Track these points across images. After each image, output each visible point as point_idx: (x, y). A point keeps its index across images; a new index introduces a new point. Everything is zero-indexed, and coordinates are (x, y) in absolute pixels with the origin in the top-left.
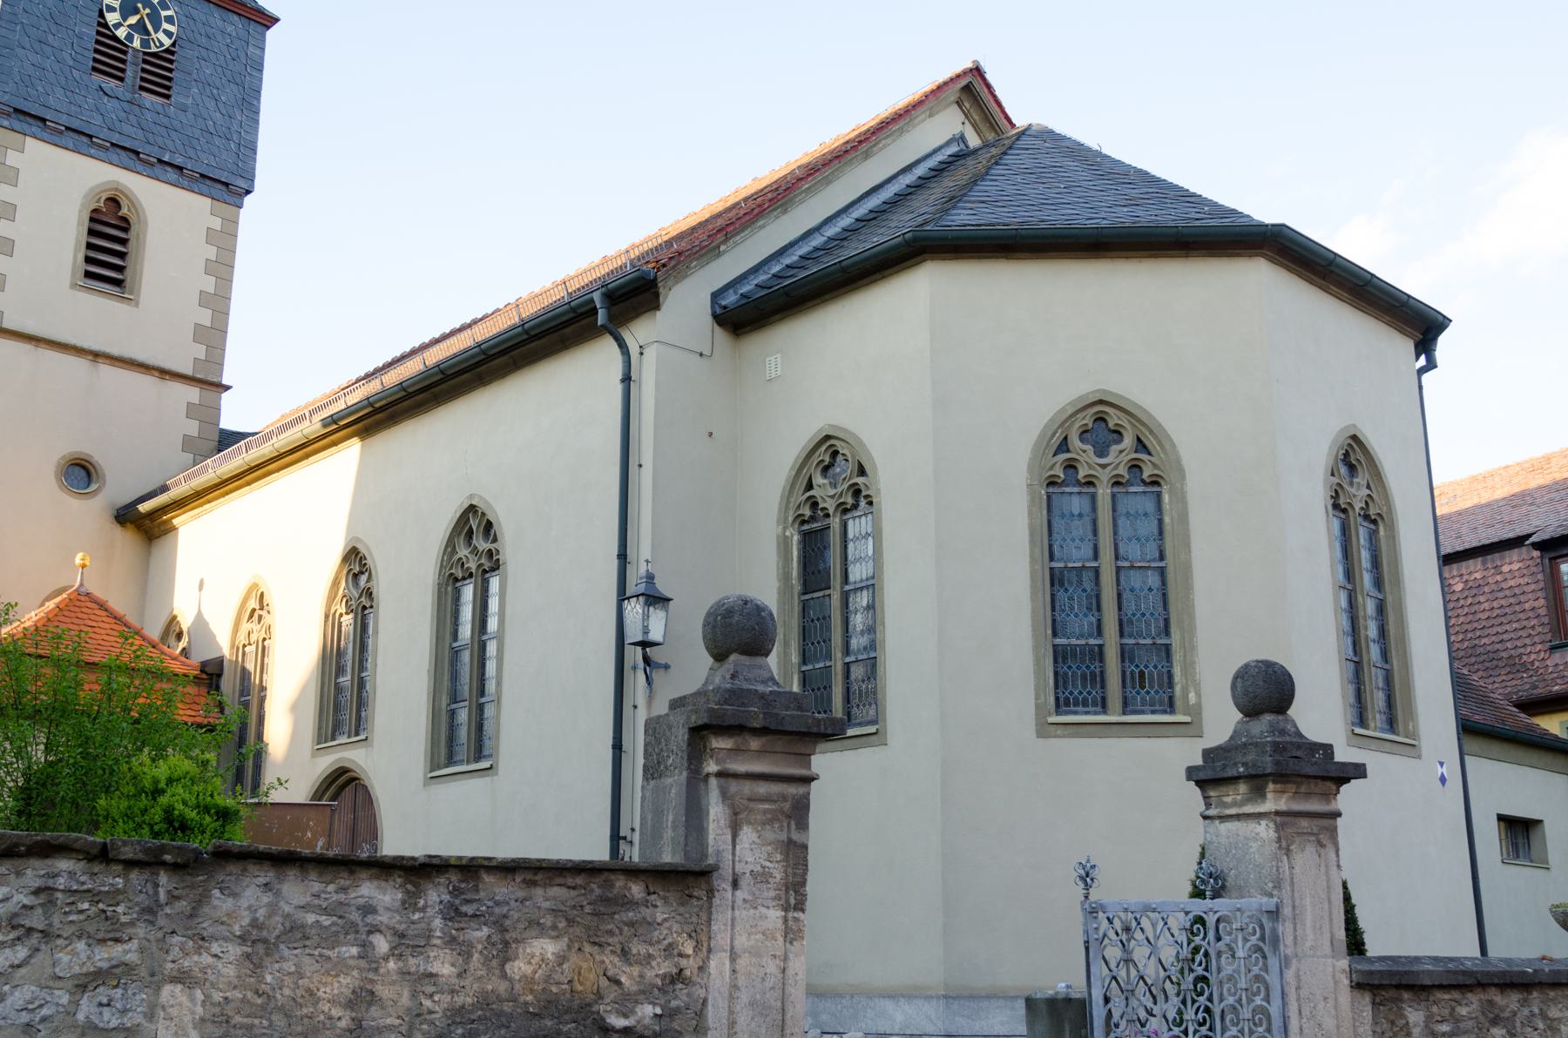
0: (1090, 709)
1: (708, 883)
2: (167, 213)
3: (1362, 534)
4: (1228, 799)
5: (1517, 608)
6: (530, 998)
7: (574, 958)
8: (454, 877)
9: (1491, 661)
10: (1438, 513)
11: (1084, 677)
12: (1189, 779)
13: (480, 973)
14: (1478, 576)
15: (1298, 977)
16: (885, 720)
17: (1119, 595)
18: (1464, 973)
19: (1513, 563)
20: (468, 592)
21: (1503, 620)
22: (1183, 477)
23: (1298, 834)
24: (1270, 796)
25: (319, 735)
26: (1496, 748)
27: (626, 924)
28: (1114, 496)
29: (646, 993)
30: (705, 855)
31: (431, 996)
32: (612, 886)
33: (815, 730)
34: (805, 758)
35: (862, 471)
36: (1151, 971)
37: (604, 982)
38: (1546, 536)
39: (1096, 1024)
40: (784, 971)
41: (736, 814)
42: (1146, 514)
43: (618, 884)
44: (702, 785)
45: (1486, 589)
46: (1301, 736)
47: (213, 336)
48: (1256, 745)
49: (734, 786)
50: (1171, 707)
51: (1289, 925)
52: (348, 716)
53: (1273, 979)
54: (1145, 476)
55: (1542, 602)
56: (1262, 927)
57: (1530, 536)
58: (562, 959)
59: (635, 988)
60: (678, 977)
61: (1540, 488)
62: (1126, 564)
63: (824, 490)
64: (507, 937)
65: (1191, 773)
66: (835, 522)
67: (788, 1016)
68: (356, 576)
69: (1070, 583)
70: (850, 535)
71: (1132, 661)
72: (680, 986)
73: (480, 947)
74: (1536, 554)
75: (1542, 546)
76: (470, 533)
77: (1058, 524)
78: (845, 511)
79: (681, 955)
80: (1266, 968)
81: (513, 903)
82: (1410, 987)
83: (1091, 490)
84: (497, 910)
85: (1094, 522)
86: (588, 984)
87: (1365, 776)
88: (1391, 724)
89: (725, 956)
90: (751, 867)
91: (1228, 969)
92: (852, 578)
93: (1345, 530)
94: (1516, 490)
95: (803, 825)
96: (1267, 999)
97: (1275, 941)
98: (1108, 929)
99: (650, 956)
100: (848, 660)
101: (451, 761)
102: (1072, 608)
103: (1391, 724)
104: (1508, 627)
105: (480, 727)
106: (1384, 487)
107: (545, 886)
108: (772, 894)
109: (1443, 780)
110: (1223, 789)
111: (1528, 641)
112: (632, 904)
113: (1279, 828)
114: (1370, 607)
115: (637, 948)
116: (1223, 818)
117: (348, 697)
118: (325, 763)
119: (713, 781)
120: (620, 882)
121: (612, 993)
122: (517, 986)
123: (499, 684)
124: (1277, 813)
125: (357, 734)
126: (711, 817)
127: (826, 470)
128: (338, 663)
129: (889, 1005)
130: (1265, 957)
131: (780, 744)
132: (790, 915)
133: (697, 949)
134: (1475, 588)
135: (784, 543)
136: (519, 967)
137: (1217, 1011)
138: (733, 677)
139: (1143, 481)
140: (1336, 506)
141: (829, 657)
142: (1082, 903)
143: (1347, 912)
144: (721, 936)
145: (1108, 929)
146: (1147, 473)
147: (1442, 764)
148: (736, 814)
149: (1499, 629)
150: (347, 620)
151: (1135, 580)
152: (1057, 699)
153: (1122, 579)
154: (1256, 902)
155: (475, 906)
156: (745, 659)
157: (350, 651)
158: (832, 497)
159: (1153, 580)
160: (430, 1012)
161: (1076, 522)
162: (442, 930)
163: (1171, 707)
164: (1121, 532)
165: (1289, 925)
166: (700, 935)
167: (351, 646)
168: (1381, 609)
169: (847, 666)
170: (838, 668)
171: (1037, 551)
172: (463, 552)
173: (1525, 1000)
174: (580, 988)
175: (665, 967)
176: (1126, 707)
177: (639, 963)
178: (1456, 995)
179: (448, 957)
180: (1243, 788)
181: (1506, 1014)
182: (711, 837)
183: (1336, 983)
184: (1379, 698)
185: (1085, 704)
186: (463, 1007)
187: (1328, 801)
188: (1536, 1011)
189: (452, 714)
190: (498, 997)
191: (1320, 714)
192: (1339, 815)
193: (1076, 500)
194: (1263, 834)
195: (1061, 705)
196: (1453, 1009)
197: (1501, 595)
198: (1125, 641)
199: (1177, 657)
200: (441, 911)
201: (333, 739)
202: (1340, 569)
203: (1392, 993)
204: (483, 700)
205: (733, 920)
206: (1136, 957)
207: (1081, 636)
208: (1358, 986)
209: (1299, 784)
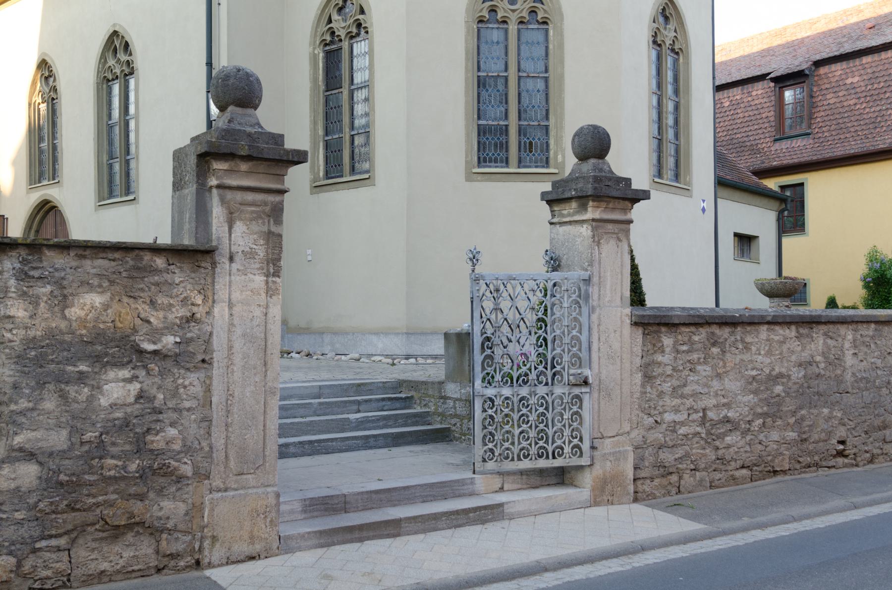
0: (499, 164)
1: (212, 258)
3: (669, 61)
4: (565, 212)
5: (758, 117)
6: (84, 332)
7: (116, 306)
8: (23, 252)
9: (741, 147)
10: (716, 61)
11: (496, 145)
12: (542, 199)
13: (46, 316)
14: (738, 97)
15: (599, 319)
16: (374, 170)
17: (519, 94)
18: (699, 316)
19: (759, 90)
20: (116, 89)
21: (750, 124)
22: (562, 19)
23: (605, 233)
24: (590, 209)
25: (30, 180)
26: (738, 195)
27: (153, 284)
28: (519, 30)
29: (169, 328)
30: (210, 240)
31: (11, 330)
32: (142, 259)
33: (285, 158)
34: (281, 177)
35: (362, 12)
36: (512, 316)
37: (138, 322)
38: (778, 74)
39: (475, 347)
40: (266, 314)
41: (231, 213)
42: (538, 43)
43: (146, 258)
44: (207, 194)
45: (742, 105)
46: (612, 172)
48: (584, 178)
49: (229, 195)
50: (547, 164)
51: (596, 288)
52: (48, 167)
53: (584, 319)
54: (539, 18)
55: (772, 113)
56: (580, 290)
57: (769, 74)
58: (106, 307)
59: (161, 325)
60: (192, 318)
61: (779, 46)
62: (525, 74)
63: (340, 25)
64: (65, 292)
65: (544, 195)
66: (345, 45)
67: (269, 343)
68: (46, 78)
69: (490, 86)
70: (355, 53)
71: (525, 135)
72: (193, 324)
73: (45, 298)
74: (772, 84)
75: (776, 80)
76: (115, 51)
77: (483, 47)
78: (352, 37)
79: (193, 304)
80: (580, 314)
81: (68, 270)
82: (666, 325)
83: (505, 26)
84: (57, 274)
85: (506, 47)
86: (127, 323)
87: (649, 198)
88: (677, 177)
89: (225, 306)
90: (243, 248)
91: (558, 314)
92: (355, 81)
93: (659, 57)
94: (765, 47)
95: (278, 221)
96: (580, 332)
97: (587, 297)
98: (485, 289)
99: (171, 305)
100: (353, 133)
101: (111, 195)
102: (490, 102)
103: (677, 177)
104: (752, 128)
105: (128, 175)
106: (685, 32)
107: (92, 259)
108: (257, 266)
109: (704, 210)
110: (563, 206)
111: (762, 136)
112: (157, 271)
113: (594, 229)
114: (670, 106)
115: (161, 300)
116: (561, 224)
117: (47, 157)
118: (36, 197)
119: (215, 191)
120: (147, 257)
121: (145, 328)
122: (74, 324)
123: (137, 147)
124: (593, 220)
125: (54, 179)
126: (214, 215)
127: (340, 10)
128: (39, 134)
129: (374, 338)
130: (580, 307)
131: (262, 167)
132: (270, 279)
133: (205, 300)
134: (735, 105)
135: (314, 58)
136: (74, 312)
137: (549, 338)
138: (230, 121)
139: (537, 21)
140: (655, 42)
141: (341, 131)
142: (471, 275)
143: (633, 283)
144: (222, 292)
145: (485, 289)
146: (540, 15)
147: (704, 201)
148: (231, 213)
149: (747, 129)
150: (43, 107)
151: (529, 84)
152: (479, 158)
153: (522, 84)
154: (577, 274)
155: (40, 271)
156: (239, 110)
157: (46, 127)
158: (343, 28)
159: (541, 85)
160: (11, 341)
161: (495, 47)
162: (16, 287)
163: (547, 164)
164: (522, 54)
165: (596, 288)
166: (208, 293)
167: (46, 124)
168: (677, 108)
169: (352, 137)
170: (347, 138)
171: (470, 64)
172: (111, 62)
173: (733, 332)
174: (120, 325)
175: (182, 312)
176: (520, 163)
177: (163, 309)
178: (693, 329)
179: (22, 305)
180: (574, 204)
181: (721, 340)
182: (214, 228)
183: (622, 322)
184: (670, 164)
185: (496, 161)
186: (34, 338)
187: (626, 214)
188: (739, 338)
189: (111, 166)
190: (60, 331)
191: (630, 160)
192: (632, 222)
193: (495, 32)
194: (584, 234)
195: (482, 161)
196: (690, 337)
197: (750, 109)
198: (521, 123)
199: (552, 133)
200: (14, 275)
201: (40, 182)
202: (654, 82)
203: (655, 328)
204: (128, 157)
205: (230, 282)
206: (502, 306)
207: (495, 119)
208: (636, 324)
209: (608, 203)
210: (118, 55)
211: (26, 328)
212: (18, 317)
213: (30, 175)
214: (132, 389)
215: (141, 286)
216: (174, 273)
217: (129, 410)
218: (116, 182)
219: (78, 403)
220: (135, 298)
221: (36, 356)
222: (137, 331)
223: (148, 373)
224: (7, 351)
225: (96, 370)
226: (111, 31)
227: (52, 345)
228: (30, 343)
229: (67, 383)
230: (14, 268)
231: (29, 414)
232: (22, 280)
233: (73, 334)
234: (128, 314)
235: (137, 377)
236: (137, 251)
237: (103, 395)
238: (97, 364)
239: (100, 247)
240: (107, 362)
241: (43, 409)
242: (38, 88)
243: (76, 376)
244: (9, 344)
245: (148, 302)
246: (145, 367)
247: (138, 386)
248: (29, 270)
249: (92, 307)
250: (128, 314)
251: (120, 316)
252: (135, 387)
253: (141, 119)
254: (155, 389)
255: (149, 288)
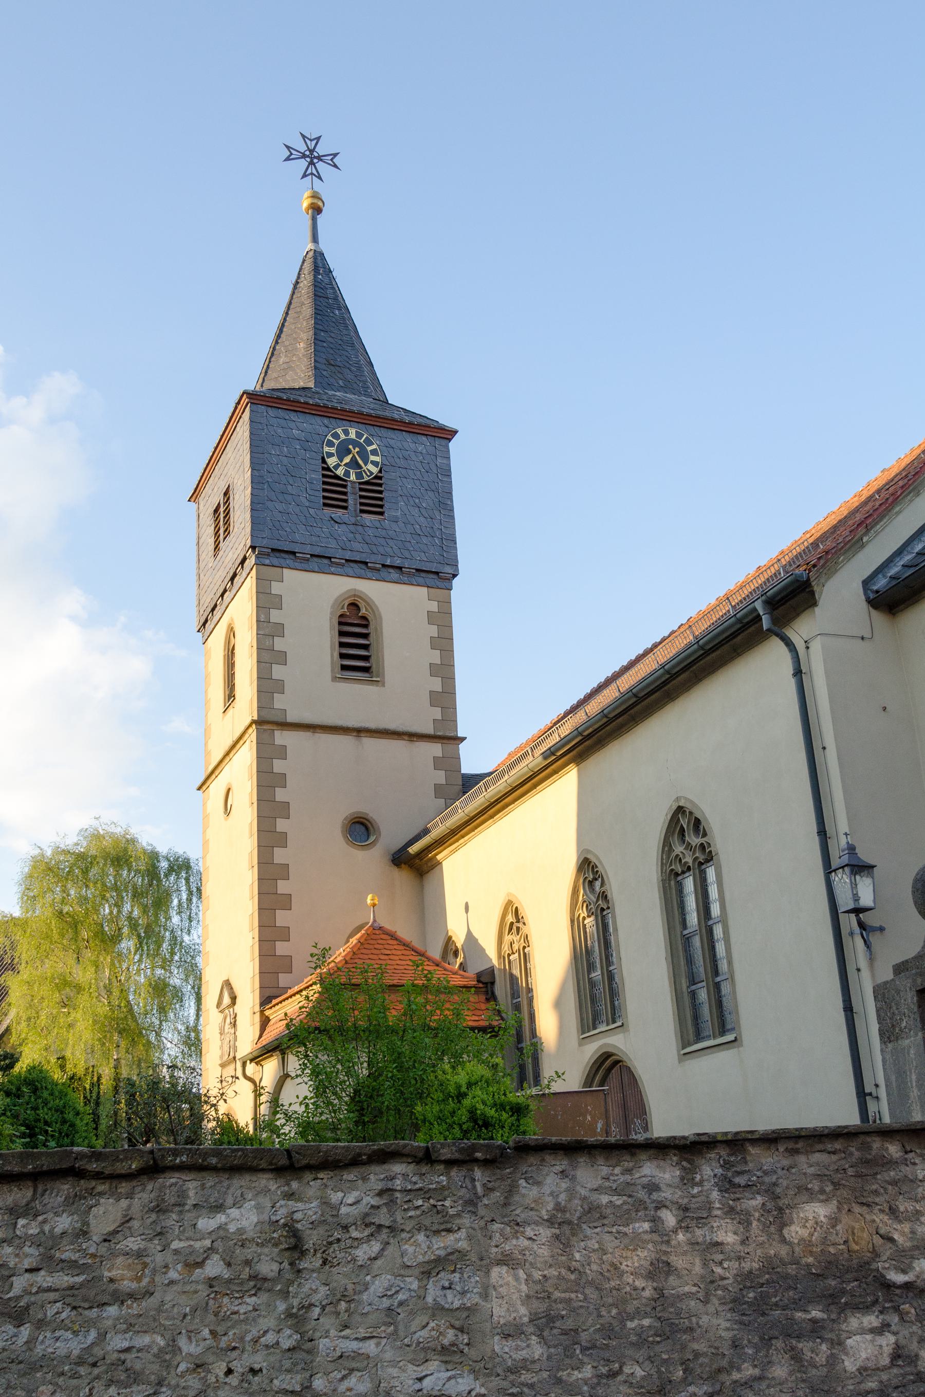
2: (395, 604)
6: (810, 1260)
7: (846, 1219)
8: (723, 1152)
20: (689, 884)
27: (890, 1183)
31: (721, 1263)
32: (870, 1148)
37: (878, 1240)
47: (445, 699)
52: (604, 1006)
58: (834, 1221)
59: (909, 1244)
64: (781, 1203)
84: (767, 1179)
86: (863, 1243)
101: (699, 1038)
105: (720, 1004)
107: (807, 1153)
112: (891, 1163)
115: (903, 1205)
117: (602, 990)
118: (592, 1050)
122: (797, 1249)
123: (730, 963)
125: (614, 1022)
128: (588, 961)
136: (796, 1232)
150: (590, 921)
155: (746, 1177)
160: (723, 1279)
172: (679, 849)
174: (856, 1248)
177: (908, 1219)
179: (730, 1227)
186: (750, 1272)
189: (693, 995)
190: (781, 1260)
200: (716, 1184)
201: (595, 1028)
204: (718, 979)
210: (687, 838)
211: (739, 1258)
212: (728, 1244)
213: (582, 1019)
214: (884, 1343)
215: (874, 1187)
216: (914, 1164)
217: (884, 1377)
218: (706, 1016)
219: (816, 1367)
220: (868, 1206)
221: (755, 1298)
222: (878, 1255)
223: (902, 1319)
224: (720, 1292)
225: (833, 1316)
226: (674, 808)
227: (773, 1282)
228: (747, 1279)
229: (799, 1337)
230: (715, 1175)
231: (756, 1385)
232: (726, 1191)
233: (798, 1263)
234: (863, 1229)
235: (889, 1325)
236: (862, 1137)
237: (847, 1354)
238: (832, 1307)
239: (815, 1136)
240: (846, 1304)
241: (773, 1378)
242: (581, 898)
243: (809, 1327)
244: (721, 1283)
245: (887, 1210)
246: (896, 1309)
247: (892, 1339)
248: (733, 1177)
249: (817, 1223)
250: (863, 1229)
251: (853, 1233)
252: (888, 1341)
253: (731, 923)
254: (915, 1343)
255: (885, 1189)
